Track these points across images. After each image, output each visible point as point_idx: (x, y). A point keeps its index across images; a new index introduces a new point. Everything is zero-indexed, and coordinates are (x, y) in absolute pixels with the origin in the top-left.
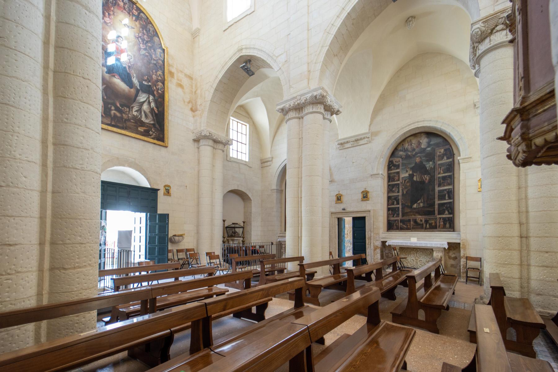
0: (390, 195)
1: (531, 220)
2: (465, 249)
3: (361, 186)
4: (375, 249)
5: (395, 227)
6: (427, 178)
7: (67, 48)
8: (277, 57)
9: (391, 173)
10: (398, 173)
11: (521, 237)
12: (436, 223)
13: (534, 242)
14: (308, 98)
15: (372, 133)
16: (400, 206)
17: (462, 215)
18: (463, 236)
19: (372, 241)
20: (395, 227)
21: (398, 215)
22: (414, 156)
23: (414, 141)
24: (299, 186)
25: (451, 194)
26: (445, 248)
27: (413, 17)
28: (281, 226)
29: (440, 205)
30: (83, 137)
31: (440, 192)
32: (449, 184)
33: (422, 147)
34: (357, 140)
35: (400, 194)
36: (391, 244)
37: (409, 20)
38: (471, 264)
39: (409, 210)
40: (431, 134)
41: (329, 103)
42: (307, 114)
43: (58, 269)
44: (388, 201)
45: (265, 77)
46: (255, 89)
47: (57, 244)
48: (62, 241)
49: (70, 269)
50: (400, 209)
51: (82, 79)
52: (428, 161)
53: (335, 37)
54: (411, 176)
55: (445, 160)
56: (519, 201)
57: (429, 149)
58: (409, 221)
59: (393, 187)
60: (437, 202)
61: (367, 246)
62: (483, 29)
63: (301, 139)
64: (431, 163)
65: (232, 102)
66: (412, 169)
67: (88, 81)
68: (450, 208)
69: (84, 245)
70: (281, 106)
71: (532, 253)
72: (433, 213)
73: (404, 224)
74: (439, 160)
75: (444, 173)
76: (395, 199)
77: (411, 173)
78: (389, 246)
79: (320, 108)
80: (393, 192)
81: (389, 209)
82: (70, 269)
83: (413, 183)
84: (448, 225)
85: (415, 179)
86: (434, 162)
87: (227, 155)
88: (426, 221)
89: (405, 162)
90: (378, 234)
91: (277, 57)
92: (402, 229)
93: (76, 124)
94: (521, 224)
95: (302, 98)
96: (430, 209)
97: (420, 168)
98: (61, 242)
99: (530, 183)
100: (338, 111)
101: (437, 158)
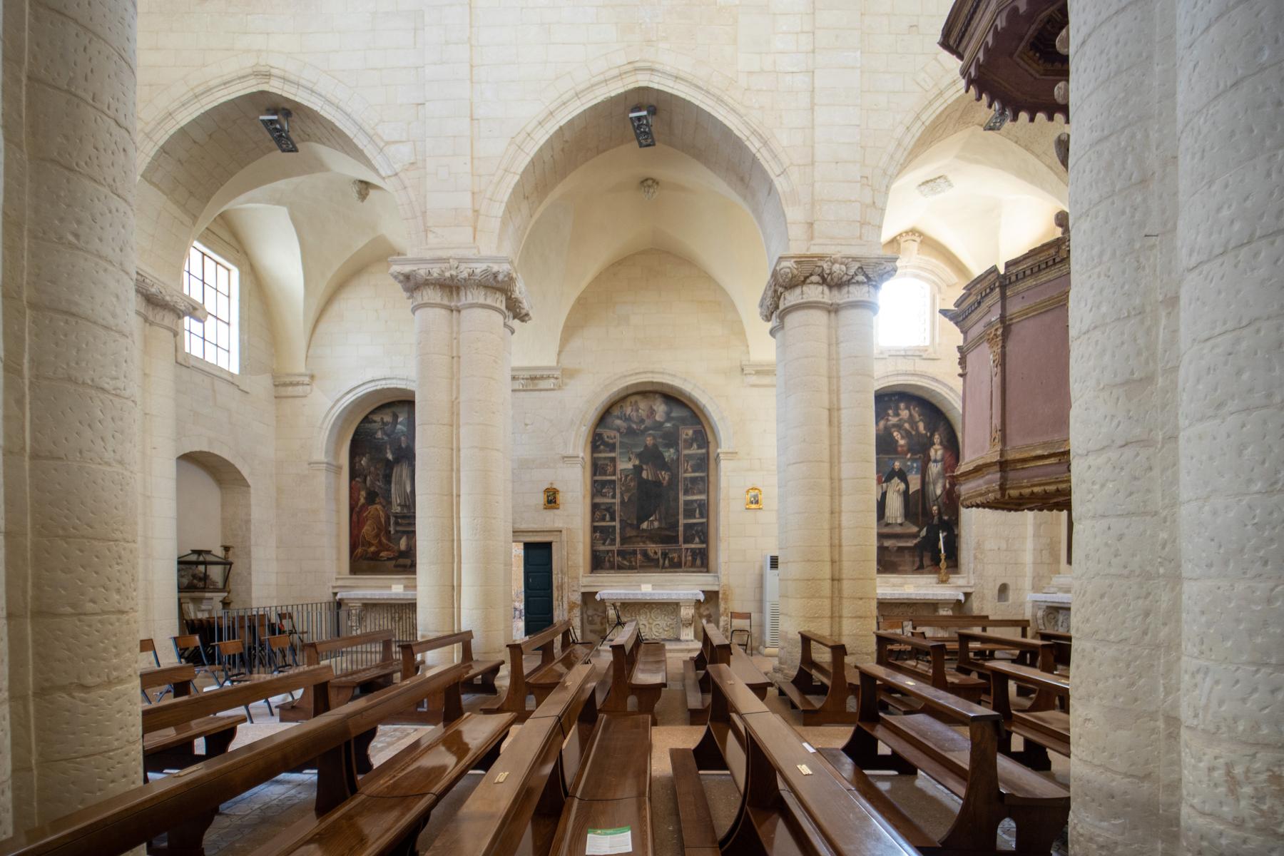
0: (597, 500)
1: (844, 558)
2: (726, 600)
3: (544, 477)
4: (571, 609)
5: (607, 564)
6: (665, 476)
7: (76, 22)
8: (387, 143)
9: (599, 458)
10: (613, 460)
11: (833, 580)
12: (680, 557)
13: (847, 586)
14: (478, 271)
15: (563, 370)
16: (617, 524)
17: (723, 546)
18: (724, 580)
19: (565, 592)
20: (607, 564)
21: (613, 540)
22: (643, 432)
23: (643, 405)
24: (453, 469)
25: (704, 509)
26: (699, 601)
27: (655, 182)
28: (338, 559)
29: (687, 526)
30: (117, 297)
31: (686, 503)
32: (700, 493)
33: (658, 418)
34: (533, 378)
35: (617, 500)
36: (605, 597)
37: (647, 183)
38: (738, 623)
39: (634, 533)
40: (672, 398)
41: (517, 294)
42: (472, 306)
43: (63, 688)
44: (593, 513)
45: (317, 166)
46: (282, 184)
47: (55, 615)
48: (73, 606)
49: (98, 686)
50: (618, 530)
51: (113, 123)
52: (668, 446)
53: (532, 162)
54: (638, 469)
55: (694, 450)
56: (832, 529)
57: (668, 425)
58: (634, 552)
59: (603, 487)
60: (682, 521)
61: (555, 603)
62: (795, 272)
63: (455, 358)
64: (672, 450)
65: (208, 199)
66: (639, 456)
67: (123, 131)
68: (702, 533)
69: (125, 617)
70: (407, 269)
71: (844, 601)
72: (674, 540)
73: (624, 558)
74: (686, 448)
75: (694, 471)
76: (608, 510)
77: (637, 462)
78: (602, 600)
79: (500, 302)
80: (604, 495)
81: (594, 529)
82: (98, 686)
83: (642, 483)
84: (698, 562)
85: (644, 475)
86: (677, 450)
87: (178, 348)
88: (665, 555)
89: (626, 440)
90: (577, 578)
91: (387, 143)
92: (620, 568)
93: (100, 257)
94: (833, 562)
95: (463, 266)
96: (667, 533)
97: (652, 456)
98: (69, 610)
99: (844, 507)
100: (527, 315)
101: (681, 445)
